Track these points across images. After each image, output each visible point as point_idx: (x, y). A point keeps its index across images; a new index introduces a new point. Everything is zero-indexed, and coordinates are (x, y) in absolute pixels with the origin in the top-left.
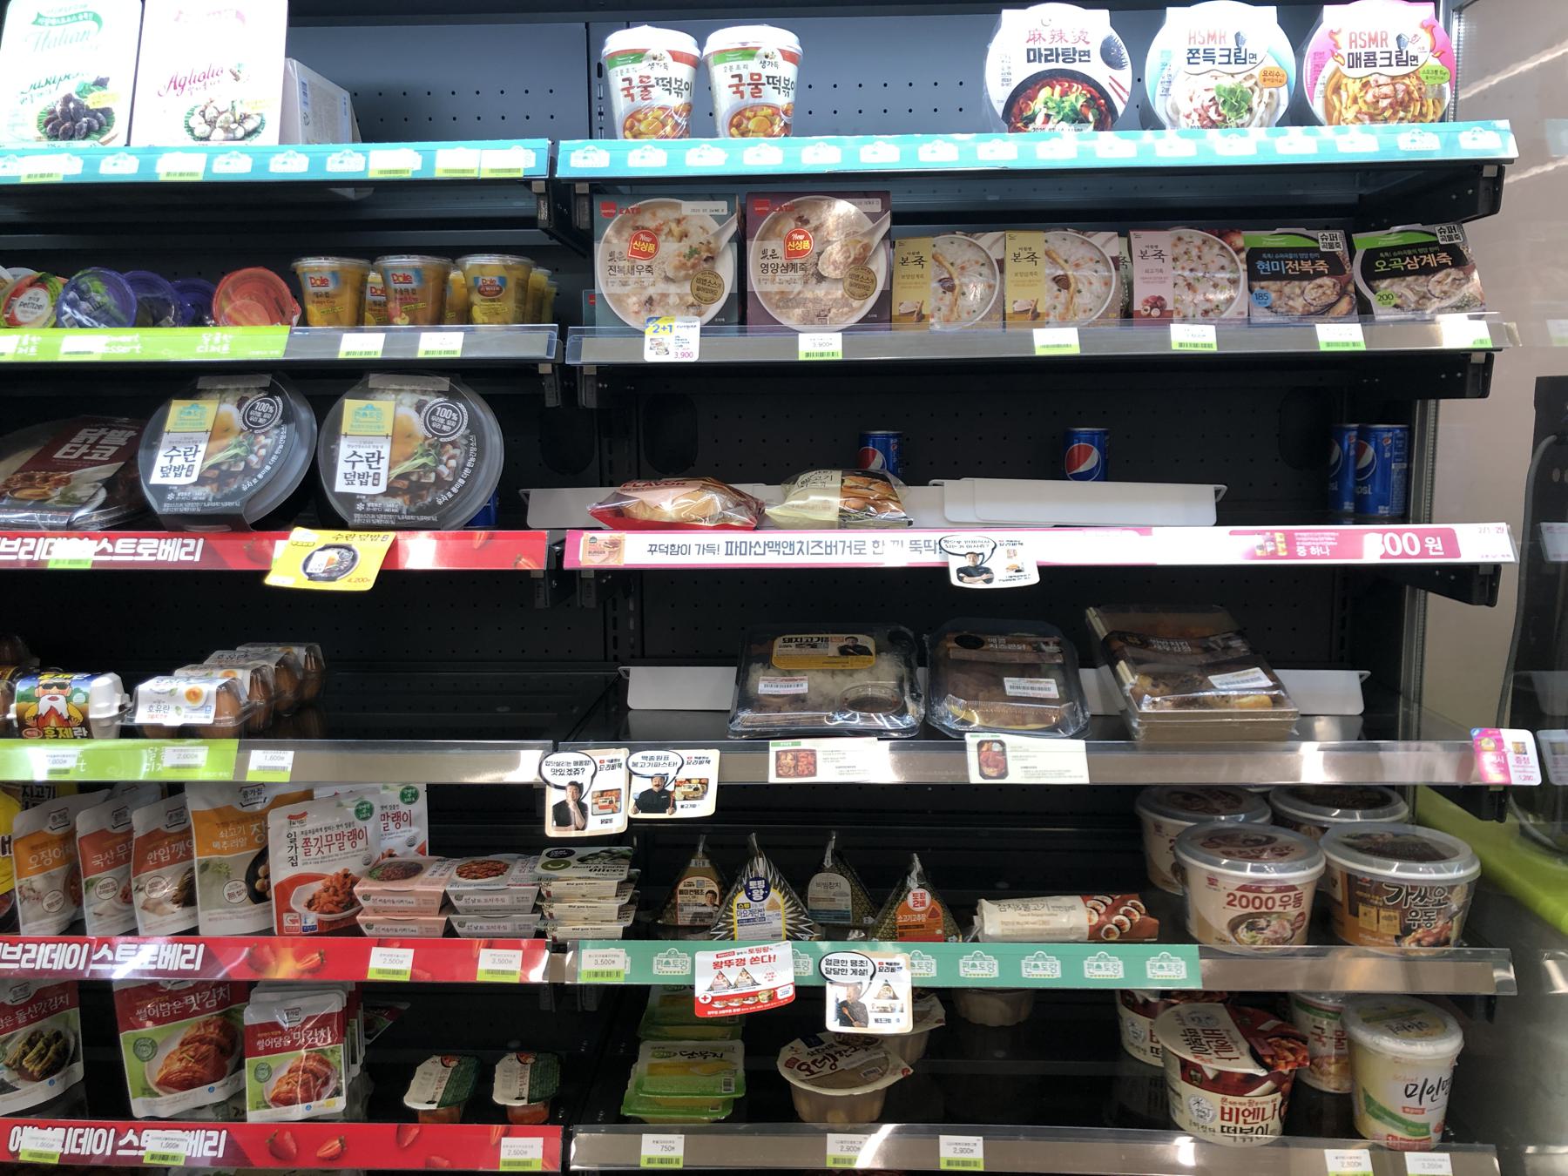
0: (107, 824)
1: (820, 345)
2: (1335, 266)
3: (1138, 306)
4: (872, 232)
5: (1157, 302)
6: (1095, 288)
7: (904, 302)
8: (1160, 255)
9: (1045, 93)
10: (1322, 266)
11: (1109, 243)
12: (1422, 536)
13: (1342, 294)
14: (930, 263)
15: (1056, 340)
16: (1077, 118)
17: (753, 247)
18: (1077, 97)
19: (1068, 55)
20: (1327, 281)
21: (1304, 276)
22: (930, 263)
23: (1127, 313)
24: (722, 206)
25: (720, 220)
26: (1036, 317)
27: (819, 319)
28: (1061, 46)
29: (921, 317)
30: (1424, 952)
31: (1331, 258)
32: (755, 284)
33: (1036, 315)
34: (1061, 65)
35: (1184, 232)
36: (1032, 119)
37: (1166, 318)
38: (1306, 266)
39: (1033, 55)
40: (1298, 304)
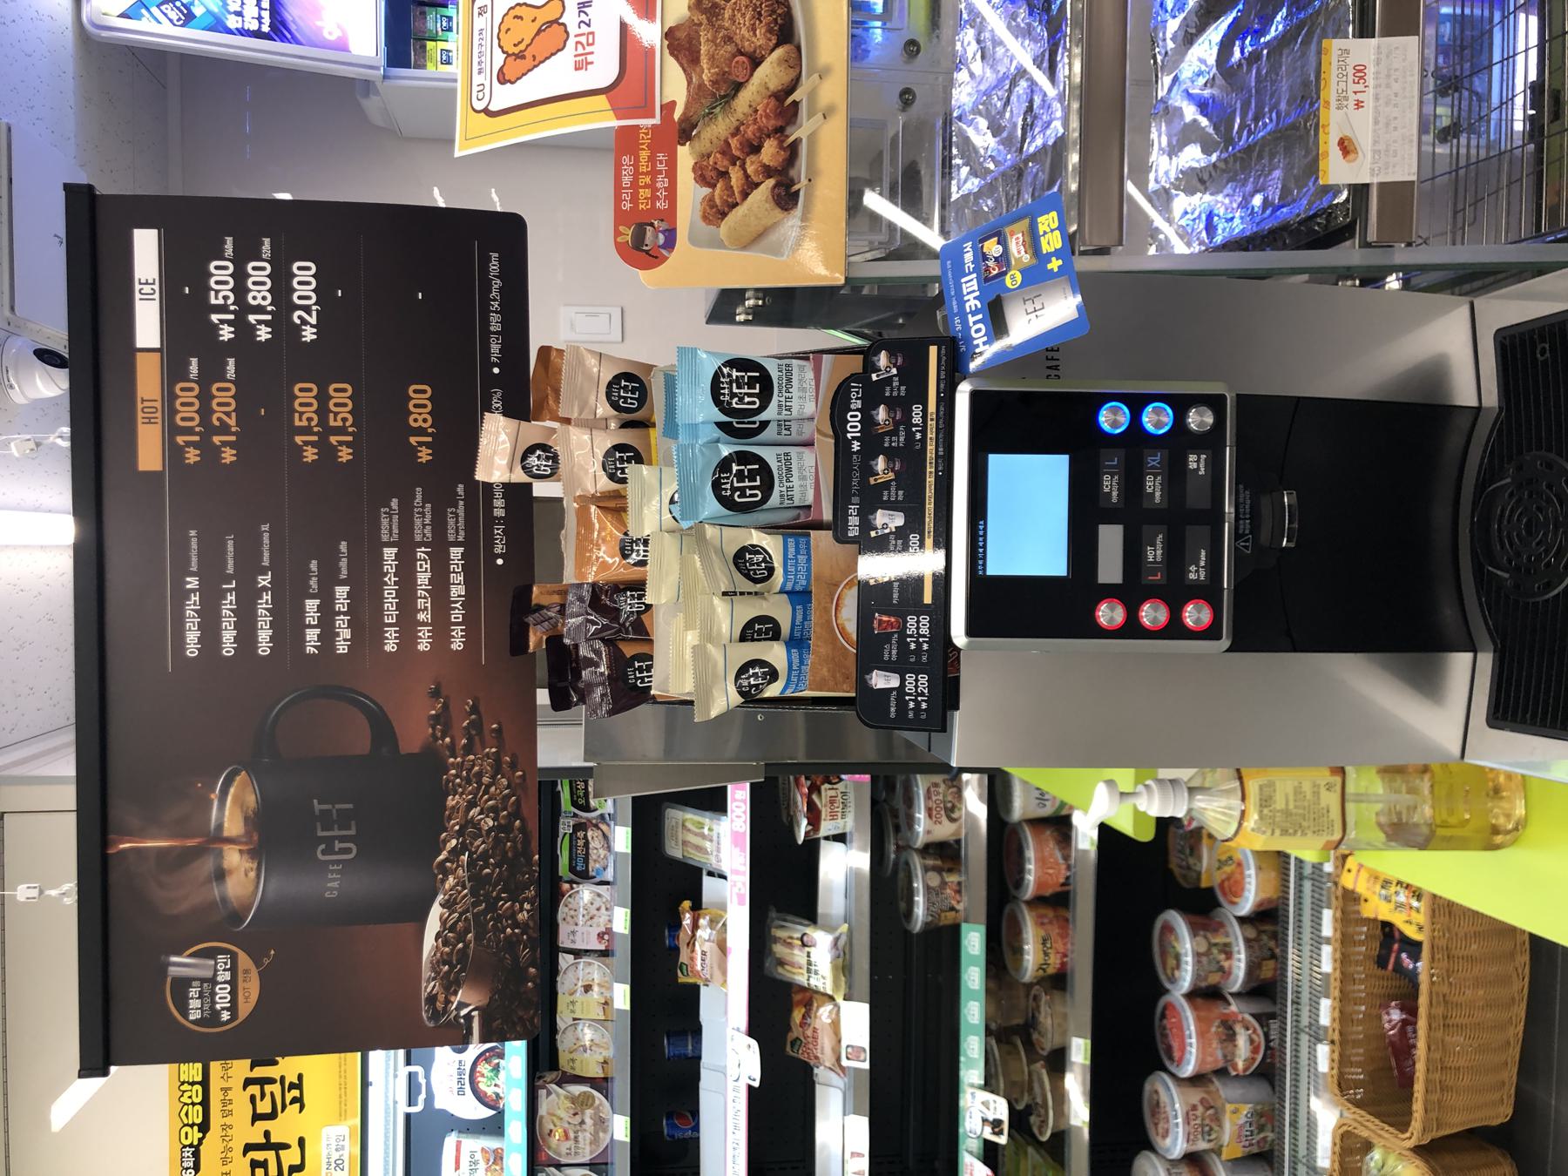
0: (1114, 460)
1: (621, 1128)
2: (580, 827)
3: (602, 947)
4: (558, 1095)
5: (600, 936)
6: (593, 971)
7: (595, 1071)
8: (573, 933)
9: (482, 1086)
10: (581, 834)
11: (565, 960)
12: (734, 800)
13: (596, 826)
14: (573, 1056)
15: (621, 996)
16: (496, 1068)
17: (564, 1161)
18: (484, 1068)
19: (460, 1073)
20: (590, 834)
21: (587, 844)
22: (573, 1056)
23: (605, 954)
24: (542, 1092)
25: (549, 1093)
26: (607, 1004)
27: (602, 1124)
28: (456, 1077)
29: (605, 1062)
30: (965, 898)
31: (577, 827)
32: (586, 1160)
33: (606, 1003)
34: (467, 1077)
35: (560, 916)
36: (497, 1095)
37: (609, 931)
38: (581, 843)
39: (461, 1092)
40: (602, 852)
